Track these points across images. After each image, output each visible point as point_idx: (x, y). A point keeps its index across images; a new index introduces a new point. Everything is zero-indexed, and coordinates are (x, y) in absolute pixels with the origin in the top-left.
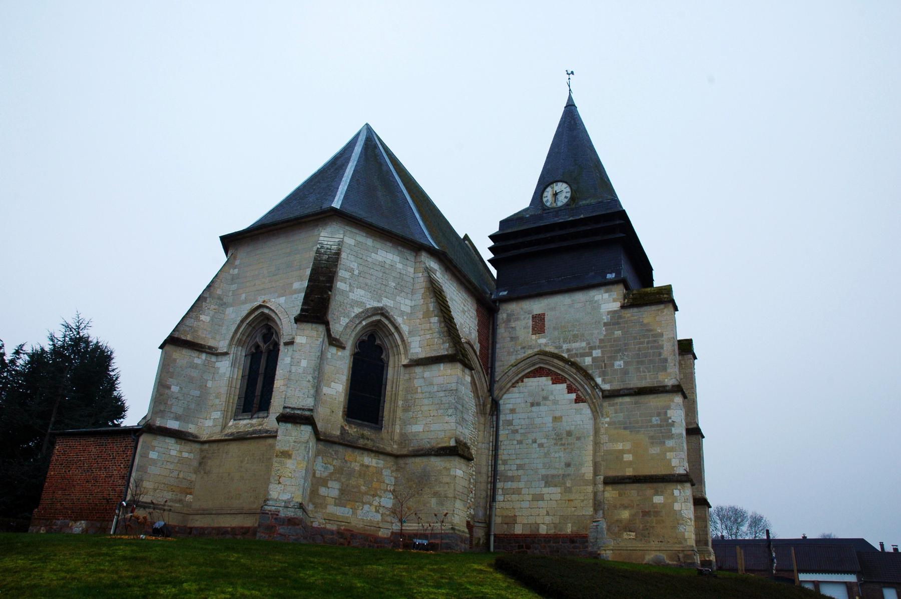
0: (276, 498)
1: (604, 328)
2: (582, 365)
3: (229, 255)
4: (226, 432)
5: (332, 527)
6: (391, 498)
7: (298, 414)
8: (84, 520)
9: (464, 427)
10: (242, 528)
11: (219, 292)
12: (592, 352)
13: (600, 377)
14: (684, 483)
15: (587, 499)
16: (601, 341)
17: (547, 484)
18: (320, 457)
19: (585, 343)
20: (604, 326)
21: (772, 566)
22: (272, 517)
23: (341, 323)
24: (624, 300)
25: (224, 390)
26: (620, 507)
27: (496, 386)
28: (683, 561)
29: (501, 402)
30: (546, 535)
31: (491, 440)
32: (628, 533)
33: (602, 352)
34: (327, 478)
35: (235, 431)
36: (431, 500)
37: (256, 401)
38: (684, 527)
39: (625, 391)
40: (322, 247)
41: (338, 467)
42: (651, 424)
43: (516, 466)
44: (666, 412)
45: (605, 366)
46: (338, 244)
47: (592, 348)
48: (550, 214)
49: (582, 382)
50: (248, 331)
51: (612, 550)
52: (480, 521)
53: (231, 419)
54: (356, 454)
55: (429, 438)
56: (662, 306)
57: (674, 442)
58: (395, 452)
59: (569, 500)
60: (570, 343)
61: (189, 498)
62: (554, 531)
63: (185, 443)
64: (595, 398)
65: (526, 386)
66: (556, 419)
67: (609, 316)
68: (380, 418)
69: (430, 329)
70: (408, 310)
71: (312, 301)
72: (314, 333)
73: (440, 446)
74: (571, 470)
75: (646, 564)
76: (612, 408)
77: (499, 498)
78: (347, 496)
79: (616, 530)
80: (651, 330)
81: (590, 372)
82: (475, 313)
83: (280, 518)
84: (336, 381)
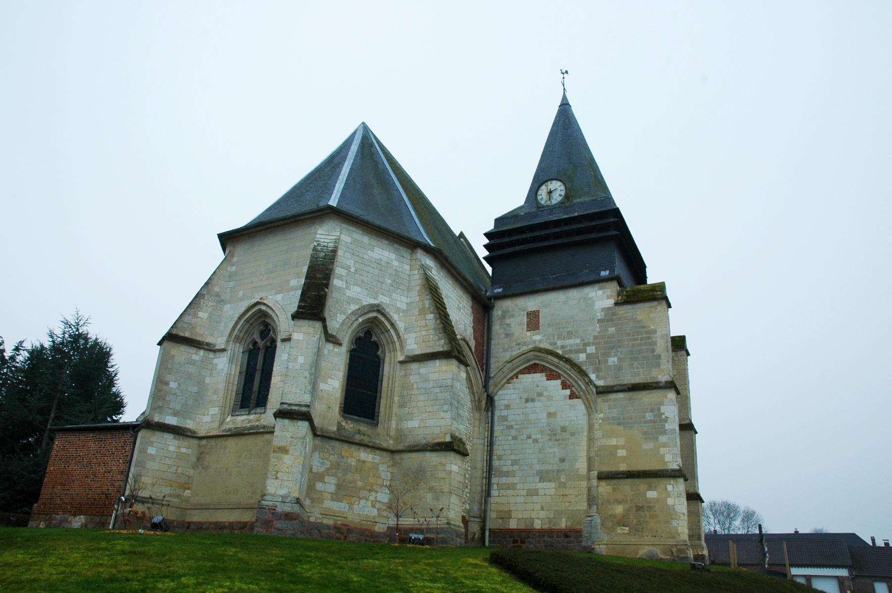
0: (273, 493)
1: (598, 325)
2: (576, 361)
3: (227, 252)
4: (224, 428)
5: (329, 522)
6: (387, 493)
7: (295, 410)
8: (83, 515)
9: (459, 423)
10: (240, 523)
11: (217, 289)
12: (586, 349)
13: (594, 373)
14: (677, 479)
15: (581, 494)
16: (595, 337)
17: (542, 479)
18: (317, 453)
19: (579, 339)
20: (598, 322)
21: (764, 560)
22: (270, 512)
23: (338, 320)
24: (618, 297)
25: (221, 386)
26: (614, 502)
27: (491, 382)
28: (676, 556)
29: (496, 398)
30: (540, 529)
31: (486, 436)
32: (622, 528)
33: (596, 349)
34: (324, 473)
35: (232, 426)
36: (426, 495)
37: (254, 397)
38: (678, 522)
39: (619, 387)
40: (319, 245)
41: (334, 462)
42: (644, 420)
43: (511, 461)
44: (660, 407)
45: (599, 362)
46: (335, 242)
47: (586, 345)
48: (545, 212)
49: (576, 379)
50: (246, 328)
51: (606, 545)
52: (475, 516)
53: (228, 415)
54: (353, 449)
55: (425, 434)
56: (655, 303)
57: (667, 438)
58: (391, 448)
59: (563, 495)
60: (564, 339)
61: (187, 493)
62: (548, 526)
63: (183, 439)
64: (589, 394)
65: (521, 383)
66: (550, 415)
67: (603, 313)
68: (376, 414)
69: (426, 326)
70: (404, 307)
71: (309, 298)
72: (311, 330)
73: (436, 441)
74: (565, 466)
75: (639, 558)
76: (606, 404)
77: (494, 493)
78: (343, 491)
79: (610, 524)
80: (645, 327)
81: (584, 368)
82: (471, 310)
83: (277, 513)
84: (333, 377)
